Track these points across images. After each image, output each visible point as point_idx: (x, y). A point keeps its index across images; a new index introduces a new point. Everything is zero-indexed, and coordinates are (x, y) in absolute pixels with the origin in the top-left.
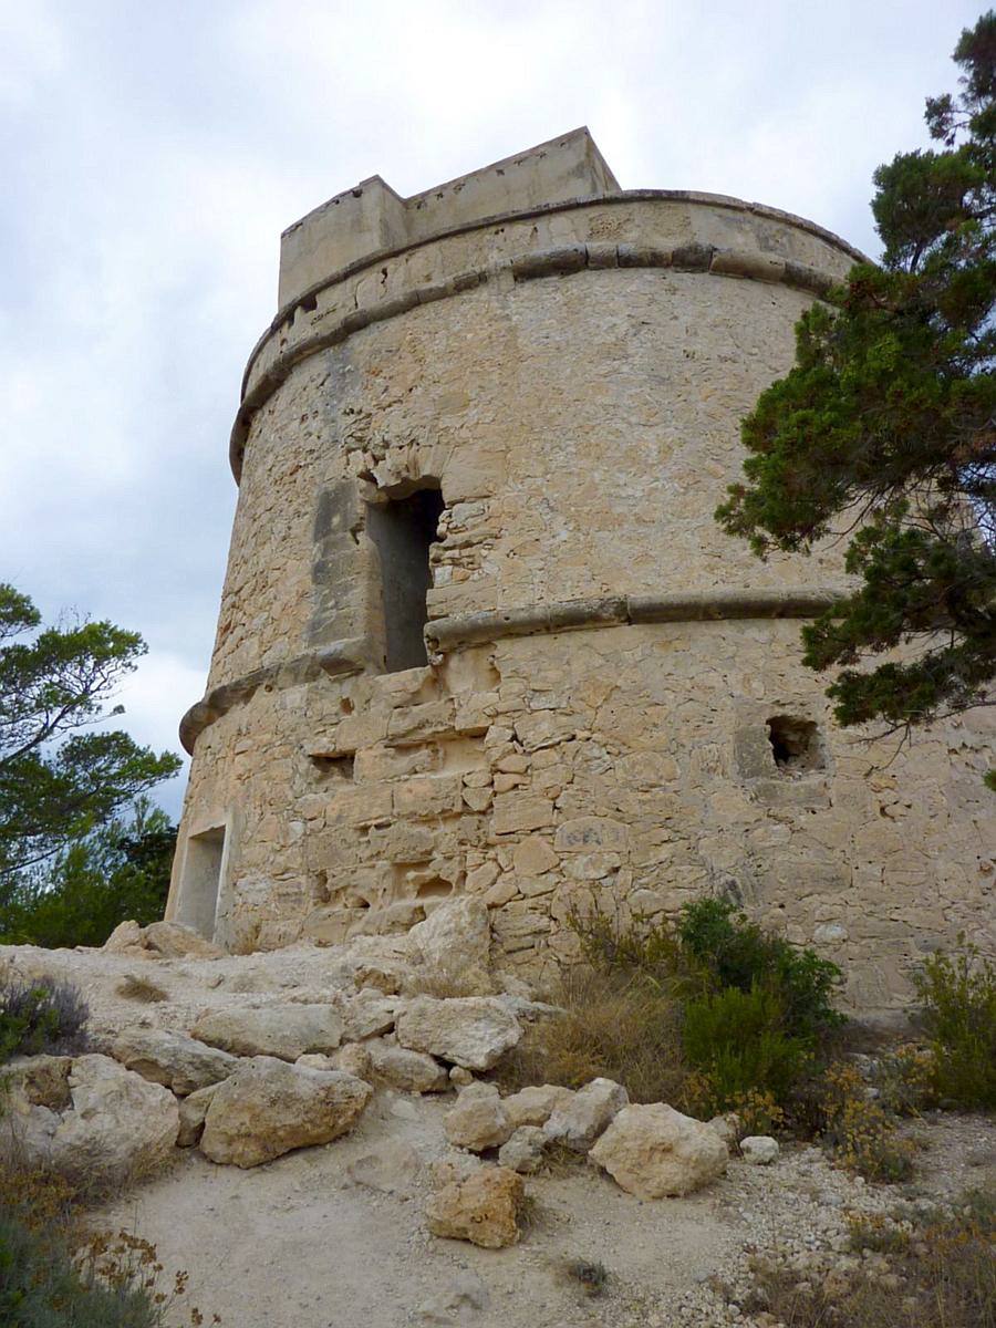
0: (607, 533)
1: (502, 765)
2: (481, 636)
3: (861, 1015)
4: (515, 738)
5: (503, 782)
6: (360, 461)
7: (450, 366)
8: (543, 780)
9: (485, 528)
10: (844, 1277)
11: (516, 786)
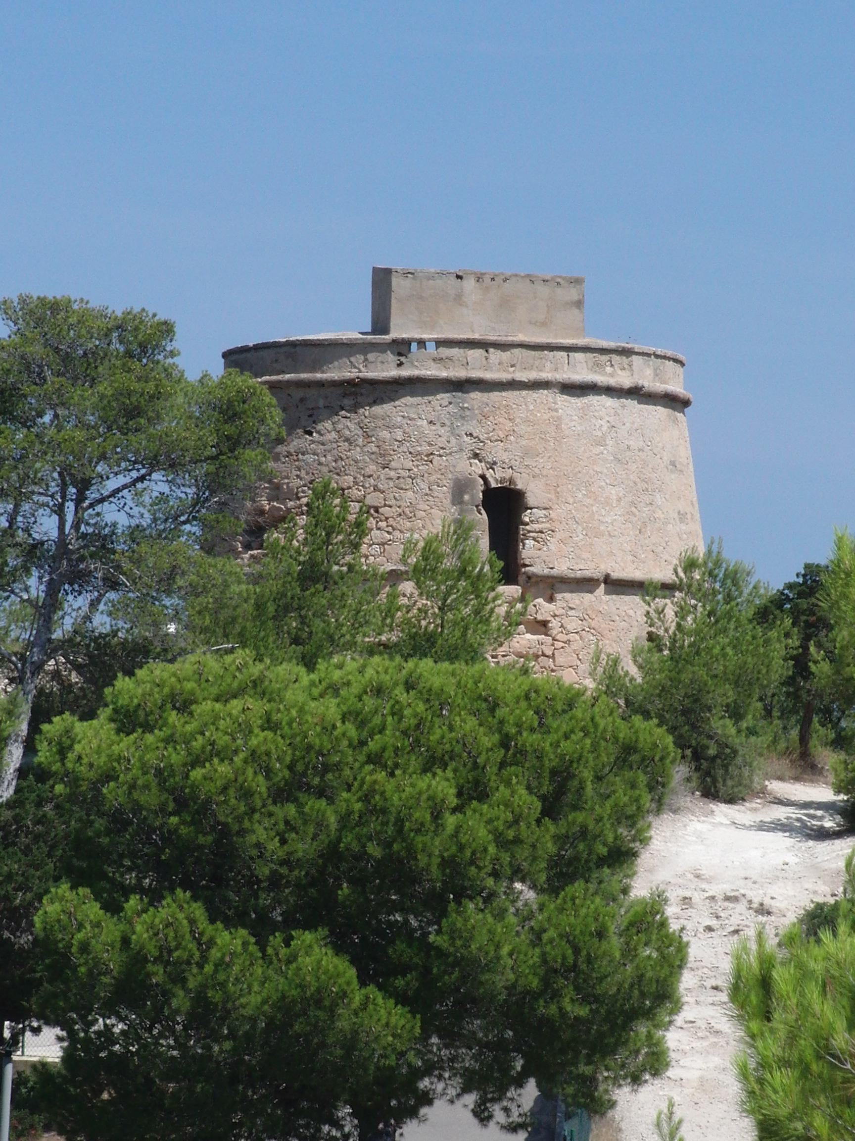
0: (609, 812)
1: (557, 638)
2: (552, 585)
3: (341, 968)
4: (562, 626)
5: (559, 645)
6: (478, 468)
7: (529, 429)
8: (574, 646)
9: (548, 525)
10: (260, 666)
11: (562, 648)
